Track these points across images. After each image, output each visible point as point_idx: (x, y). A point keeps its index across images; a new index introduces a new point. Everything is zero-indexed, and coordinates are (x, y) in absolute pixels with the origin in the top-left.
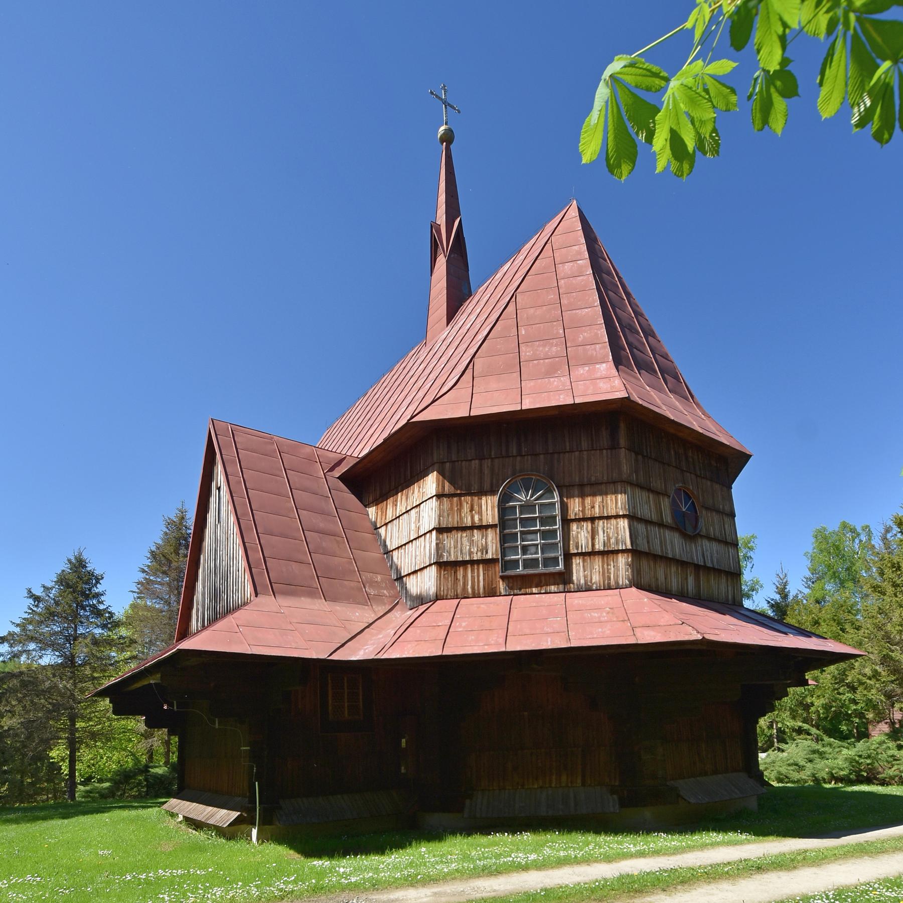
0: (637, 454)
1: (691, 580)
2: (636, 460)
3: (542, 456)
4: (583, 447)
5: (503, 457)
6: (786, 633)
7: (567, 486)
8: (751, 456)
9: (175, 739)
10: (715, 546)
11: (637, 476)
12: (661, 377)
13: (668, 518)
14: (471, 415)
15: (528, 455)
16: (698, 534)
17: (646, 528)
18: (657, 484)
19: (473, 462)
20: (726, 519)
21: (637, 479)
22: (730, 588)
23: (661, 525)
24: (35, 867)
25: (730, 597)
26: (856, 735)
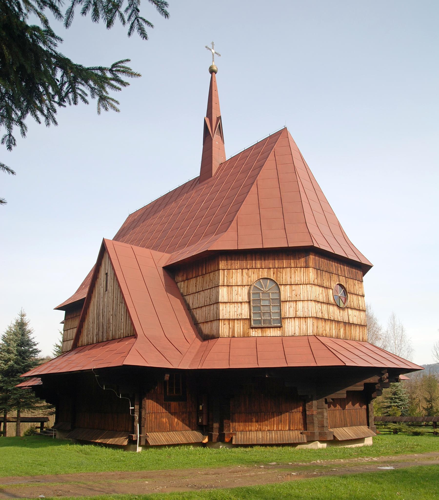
0: (317, 269)
1: (342, 330)
2: (317, 273)
3: (272, 269)
4: (292, 266)
5: (253, 269)
6: (219, 118)
7: (284, 285)
8: (372, 266)
9: (28, 409)
10: (356, 313)
11: (317, 281)
12: (273, 149)
13: (332, 300)
14: (239, 249)
15: (265, 268)
16: (346, 307)
17: (321, 306)
18: (326, 284)
19: (239, 270)
20: (360, 297)
21: (317, 282)
22: (361, 333)
23: (328, 304)
24: (214, 480)
25: (361, 339)
26: (49, 404)
